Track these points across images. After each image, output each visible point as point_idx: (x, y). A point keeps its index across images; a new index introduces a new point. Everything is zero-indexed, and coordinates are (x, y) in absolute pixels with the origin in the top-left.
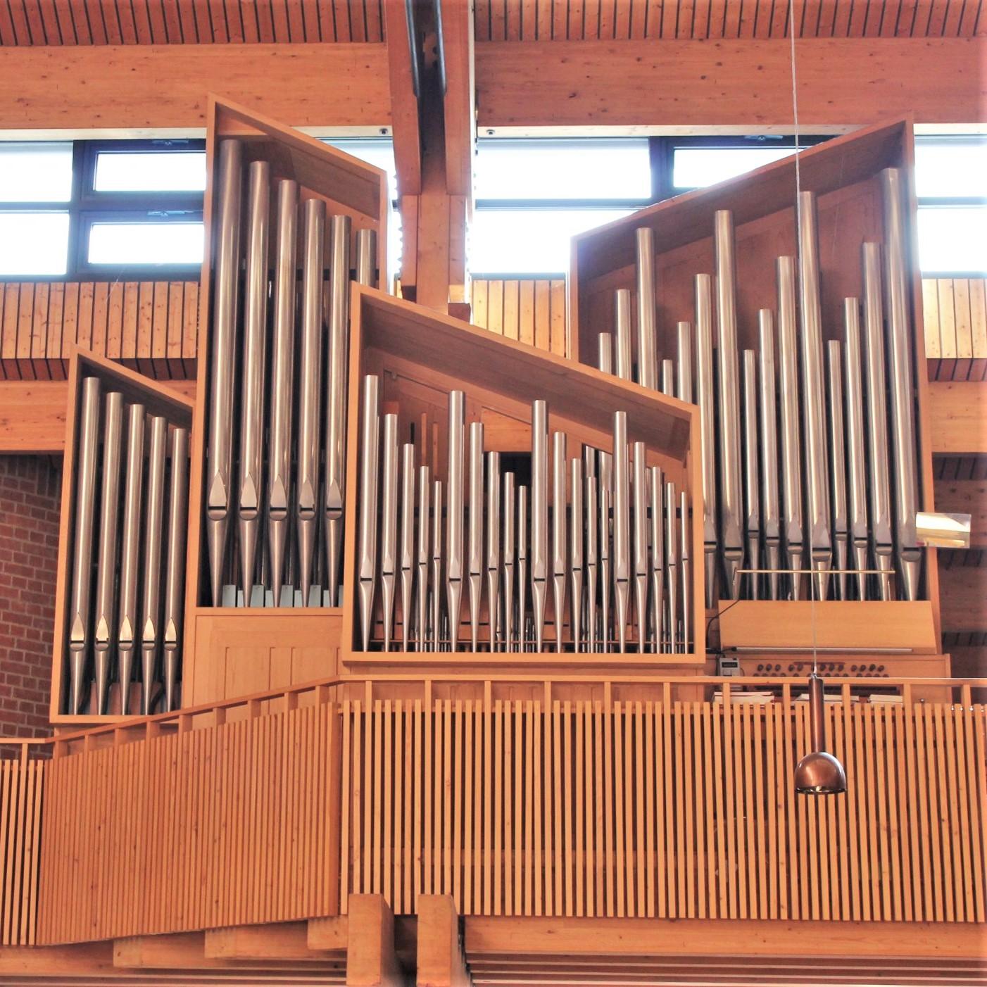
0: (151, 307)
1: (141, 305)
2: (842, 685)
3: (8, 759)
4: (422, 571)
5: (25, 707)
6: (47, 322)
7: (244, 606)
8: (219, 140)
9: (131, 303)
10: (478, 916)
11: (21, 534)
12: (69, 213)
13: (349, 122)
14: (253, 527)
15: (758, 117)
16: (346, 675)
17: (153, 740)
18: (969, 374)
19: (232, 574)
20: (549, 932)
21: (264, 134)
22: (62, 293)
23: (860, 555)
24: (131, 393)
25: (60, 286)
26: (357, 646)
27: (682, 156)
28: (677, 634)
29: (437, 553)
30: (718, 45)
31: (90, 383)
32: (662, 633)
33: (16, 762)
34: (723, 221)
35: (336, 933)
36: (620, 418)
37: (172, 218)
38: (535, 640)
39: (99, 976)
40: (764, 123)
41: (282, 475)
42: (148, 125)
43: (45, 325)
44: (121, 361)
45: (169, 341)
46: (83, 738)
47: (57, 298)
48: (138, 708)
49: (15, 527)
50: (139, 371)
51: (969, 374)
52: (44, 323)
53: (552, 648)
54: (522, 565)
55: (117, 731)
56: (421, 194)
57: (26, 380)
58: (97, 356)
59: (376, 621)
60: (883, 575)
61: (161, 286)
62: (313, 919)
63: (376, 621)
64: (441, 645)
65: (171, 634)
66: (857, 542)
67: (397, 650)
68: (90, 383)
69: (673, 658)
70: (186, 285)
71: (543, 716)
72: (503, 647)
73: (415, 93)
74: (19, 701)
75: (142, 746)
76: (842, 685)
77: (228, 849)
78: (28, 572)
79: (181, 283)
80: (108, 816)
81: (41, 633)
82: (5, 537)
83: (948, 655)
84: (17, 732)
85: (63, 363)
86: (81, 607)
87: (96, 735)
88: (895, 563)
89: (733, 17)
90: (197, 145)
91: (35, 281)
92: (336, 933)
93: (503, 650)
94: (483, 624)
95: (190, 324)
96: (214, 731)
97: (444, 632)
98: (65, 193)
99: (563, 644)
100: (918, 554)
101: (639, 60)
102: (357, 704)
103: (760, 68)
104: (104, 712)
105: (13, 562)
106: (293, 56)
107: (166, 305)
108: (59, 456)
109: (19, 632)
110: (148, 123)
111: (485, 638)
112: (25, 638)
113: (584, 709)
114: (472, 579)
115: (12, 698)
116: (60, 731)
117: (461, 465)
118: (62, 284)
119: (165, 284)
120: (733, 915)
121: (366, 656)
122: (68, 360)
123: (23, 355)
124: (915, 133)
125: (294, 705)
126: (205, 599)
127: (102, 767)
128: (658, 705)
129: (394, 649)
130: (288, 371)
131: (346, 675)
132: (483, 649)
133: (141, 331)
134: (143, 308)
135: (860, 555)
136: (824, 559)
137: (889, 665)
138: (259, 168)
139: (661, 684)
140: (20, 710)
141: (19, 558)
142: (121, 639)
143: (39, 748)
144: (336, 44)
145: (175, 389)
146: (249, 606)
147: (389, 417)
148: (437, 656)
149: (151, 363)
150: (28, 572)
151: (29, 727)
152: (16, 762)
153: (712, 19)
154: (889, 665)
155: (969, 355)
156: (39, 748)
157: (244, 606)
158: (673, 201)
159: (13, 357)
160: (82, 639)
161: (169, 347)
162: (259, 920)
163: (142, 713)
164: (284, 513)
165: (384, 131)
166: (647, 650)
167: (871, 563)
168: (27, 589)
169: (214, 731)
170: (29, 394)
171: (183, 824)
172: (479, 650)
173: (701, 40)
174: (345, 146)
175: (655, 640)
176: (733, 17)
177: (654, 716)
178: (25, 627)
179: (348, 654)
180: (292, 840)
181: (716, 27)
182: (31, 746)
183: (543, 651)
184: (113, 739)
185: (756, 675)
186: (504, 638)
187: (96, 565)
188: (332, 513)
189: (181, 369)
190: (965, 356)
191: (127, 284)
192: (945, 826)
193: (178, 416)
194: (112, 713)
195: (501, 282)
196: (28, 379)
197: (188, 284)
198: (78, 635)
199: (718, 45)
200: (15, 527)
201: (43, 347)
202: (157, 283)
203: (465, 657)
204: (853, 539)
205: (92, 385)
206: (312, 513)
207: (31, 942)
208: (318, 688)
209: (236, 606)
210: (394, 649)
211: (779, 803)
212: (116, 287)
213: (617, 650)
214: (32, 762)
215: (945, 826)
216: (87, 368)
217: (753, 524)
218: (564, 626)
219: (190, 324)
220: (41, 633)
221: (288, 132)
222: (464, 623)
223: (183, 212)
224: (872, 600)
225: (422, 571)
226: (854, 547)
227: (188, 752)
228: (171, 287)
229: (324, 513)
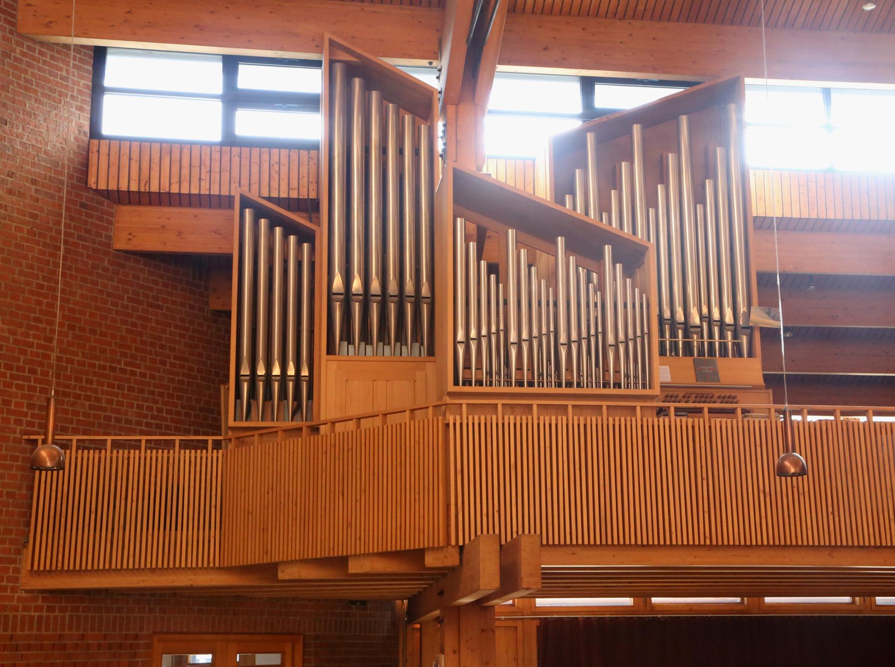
0: (278, 164)
1: (271, 164)
2: (703, 408)
3: (187, 449)
4: (593, 340)
5: (187, 415)
6: (210, 171)
7: (373, 355)
8: (332, 63)
9: (265, 161)
10: (760, 546)
11: (183, 305)
12: (222, 101)
13: (411, 57)
14: (360, 306)
15: (654, 68)
16: (448, 400)
17: (308, 438)
18: (150, 200)
19: (347, 336)
20: (573, 554)
21: (358, 60)
22: (219, 153)
23: (716, 330)
24: (275, 221)
25: (218, 148)
26: (456, 383)
27: (599, 88)
28: (539, 376)
29: (600, 330)
30: (630, 23)
31: (248, 212)
32: (634, 377)
33: (137, 452)
34: (636, 129)
35: (446, 556)
36: (608, 249)
37: (289, 109)
38: (510, 378)
39: (264, 584)
40: (655, 73)
41: (377, 274)
42: (282, 49)
43: (209, 173)
44: (264, 198)
45: (291, 187)
46: (253, 436)
47: (216, 156)
48: (269, 417)
49: (179, 300)
50: (279, 205)
51: (150, 200)
52: (207, 172)
53: (481, 384)
54: (502, 334)
55: (280, 432)
56: (458, 105)
57: (193, 207)
58: (254, 196)
59: (467, 367)
60: (668, 341)
61: (284, 152)
62: (429, 548)
63: (467, 367)
64: (539, 383)
65: (305, 372)
66: (715, 323)
67: (570, 387)
68: (248, 212)
69: (640, 391)
70: (232, 150)
71: (550, 425)
72: (491, 383)
73: (467, 42)
74: (183, 411)
75: (299, 442)
76: (703, 408)
77: (303, 508)
78: (187, 329)
79: (297, 151)
80: (275, 485)
81: (196, 368)
82: (173, 307)
83: (771, 391)
84: (192, 432)
85: (231, 198)
86: (306, 357)
87: (261, 435)
88: (735, 336)
89: (641, 7)
90: (317, 64)
91: (202, 144)
92: (446, 556)
93: (491, 385)
94: (479, 368)
95: (303, 177)
96: (354, 433)
97: (508, 375)
98: (219, 89)
99: (528, 382)
100: (749, 331)
101: (584, 29)
102: (458, 417)
103: (654, 39)
104: (246, 420)
105: (178, 323)
106: (374, 12)
107: (288, 164)
108: (229, 258)
109: (182, 367)
110: (282, 48)
111: (468, 377)
112: (185, 371)
113: (544, 421)
114: (471, 342)
115: (179, 409)
116: (232, 432)
117: (705, 282)
118: (219, 147)
119: (277, 150)
120: (610, 542)
121: (461, 388)
122: (234, 197)
123: (195, 191)
124: (746, 83)
125: (412, 418)
126: (331, 350)
127: (269, 454)
128: (530, 418)
129: (568, 385)
130: (379, 210)
131: (448, 400)
132: (467, 384)
133: (272, 180)
134: (273, 165)
135: (716, 330)
136: (697, 333)
137: (740, 396)
138: (357, 82)
139: (635, 407)
140: (184, 416)
141: (182, 320)
142: (273, 374)
143: (153, 441)
144: (401, 6)
145: (302, 217)
146: (376, 355)
147: (471, 244)
148: (504, 389)
149: (148, 195)
150: (187, 329)
151: (190, 427)
152: (204, 451)
153: (628, 8)
154: (740, 396)
155: (206, 190)
156: (153, 441)
157: (373, 355)
158: (608, 117)
159: (187, 192)
160: (248, 374)
161: (291, 191)
162: (401, 548)
163: (273, 420)
164: (361, 297)
165: (430, 63)
166: (579, 385)
167: (722, 336)
168: (187, 340)
169: (354, 433)
170: (196, 216)
171: (332, 489)
172: (464, 384)
173: (620, 19)
174: (413, 72)
175: (583, 379)
176: (641, 7)
177: (509, 424)
178: (187, 364)
179: (451, 388)
180: (415, 500)
181: (630, 12)
182: (147, 441)
183: (475, 385)
184: (277, 436)
185: (664, 402)
186: (491, 377)
187: (254, 327)
188: (408, 298)
189: (311, 207)
190: (762, 215)
191: (263, 150)
192: (795, 490)
193: (306, 236)
194: (251, 421)
195: (495, 160)
196: (195, 207)
197: (301, 151)
198: (245, 371)
199: (630, 23)
200: (179, 300)
201: (208, 187)
202: (282, 150)
203: (467, 389)
204: (712, 321)
205: (249, 213)
206: (396, 299)
207: (217, 565)
208: (431, 409)
209: (348, 354)
210: (568, 385)
211: (703, 477)
212: (255, 152)
213: (560, 385)
214: (80, 452)
215: (795, 490)
216: (246, 203)
217: (667, 314)
218: (528, 370)
219: (303, 177)
220: (196, 368)
221: (375, 61)
222: (616, 372)
223: (297, 106)
224: (689, 356)
225: (593, 340)
226: (713, 326)
227: (335, 446)
228: (291, 153)
229: (419, 300)
